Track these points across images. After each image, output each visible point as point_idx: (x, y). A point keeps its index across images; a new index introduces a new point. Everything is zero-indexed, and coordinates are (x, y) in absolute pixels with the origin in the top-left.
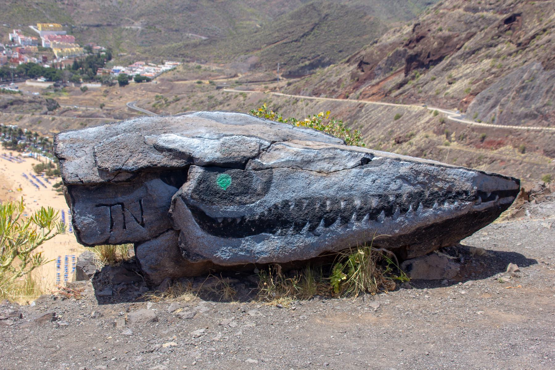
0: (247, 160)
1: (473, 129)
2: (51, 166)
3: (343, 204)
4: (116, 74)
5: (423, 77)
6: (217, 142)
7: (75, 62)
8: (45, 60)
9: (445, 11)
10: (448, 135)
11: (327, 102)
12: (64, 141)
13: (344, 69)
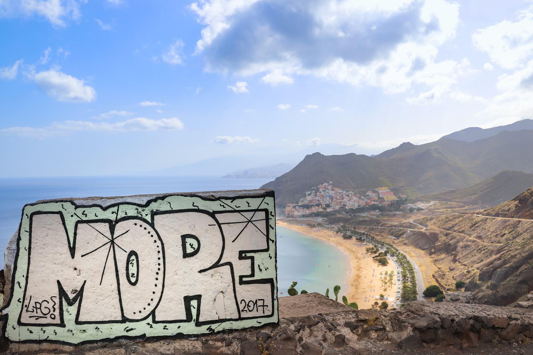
2: (373, 249)
4: (409, 208)
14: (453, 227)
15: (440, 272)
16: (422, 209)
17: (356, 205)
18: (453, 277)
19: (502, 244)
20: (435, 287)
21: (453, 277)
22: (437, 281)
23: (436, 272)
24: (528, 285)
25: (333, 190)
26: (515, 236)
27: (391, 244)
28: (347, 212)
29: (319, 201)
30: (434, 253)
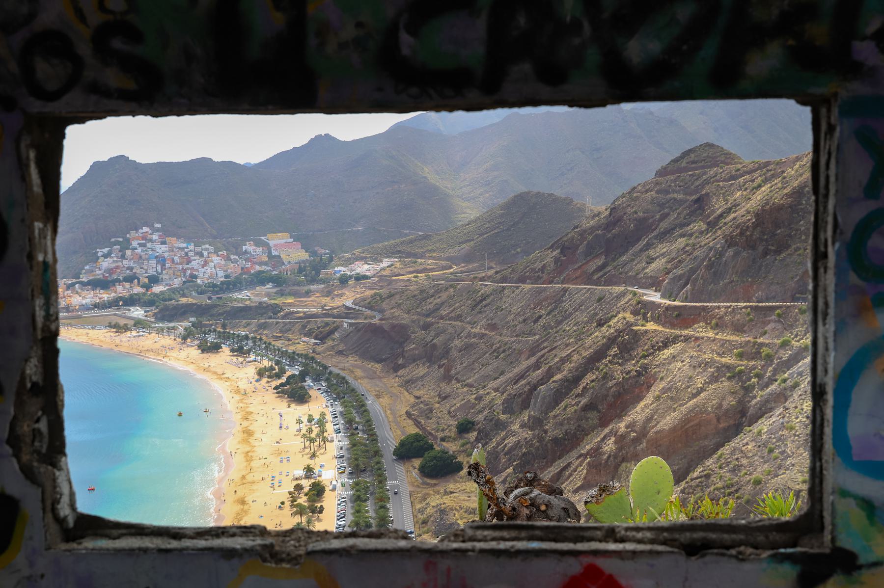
1: (668, 308)
2: (272, 368)
4: (338, 275)
14: (438, 309)
15: (422, 406)
16: (365, 277)
17: (221, 274)
18: (449, 412)
19: (537, 337)
20: (417, 438)
21: (449, 412)
22: (417, 424)
23: (413, 406)
24: (599, 411)
27: (311, 355)
29: (131, 269)
30: (403, 366)
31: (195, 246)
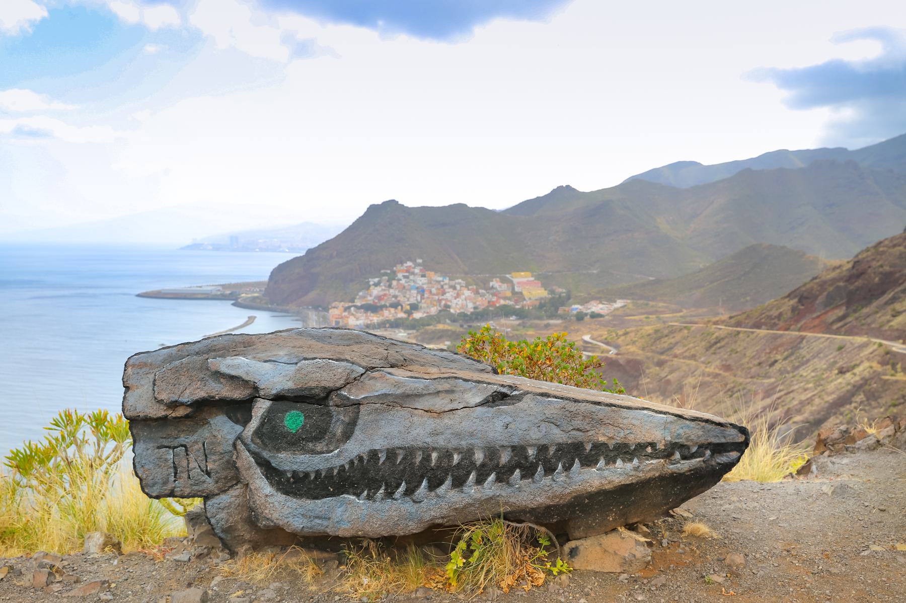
0: (329, 392)
3: (456, 458)
4: (575, 312)
5: (866, 310)
6: (293, 368)
7: (540, 303)
8: (517, 302)
9: (885, 249)
10: (894, 366)
11: (768, 334)
12: (133, 366)
13: (784, 303)
14: (671, 348)
16: (599, 316)
17: (470, 305)
19: (772, 380)
25: (423, 276)
26: (797, 364)
28: (454, 319)
29: (395, 297)
31: (450, 280)
